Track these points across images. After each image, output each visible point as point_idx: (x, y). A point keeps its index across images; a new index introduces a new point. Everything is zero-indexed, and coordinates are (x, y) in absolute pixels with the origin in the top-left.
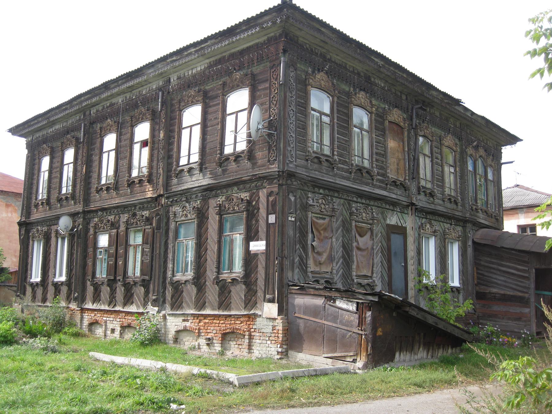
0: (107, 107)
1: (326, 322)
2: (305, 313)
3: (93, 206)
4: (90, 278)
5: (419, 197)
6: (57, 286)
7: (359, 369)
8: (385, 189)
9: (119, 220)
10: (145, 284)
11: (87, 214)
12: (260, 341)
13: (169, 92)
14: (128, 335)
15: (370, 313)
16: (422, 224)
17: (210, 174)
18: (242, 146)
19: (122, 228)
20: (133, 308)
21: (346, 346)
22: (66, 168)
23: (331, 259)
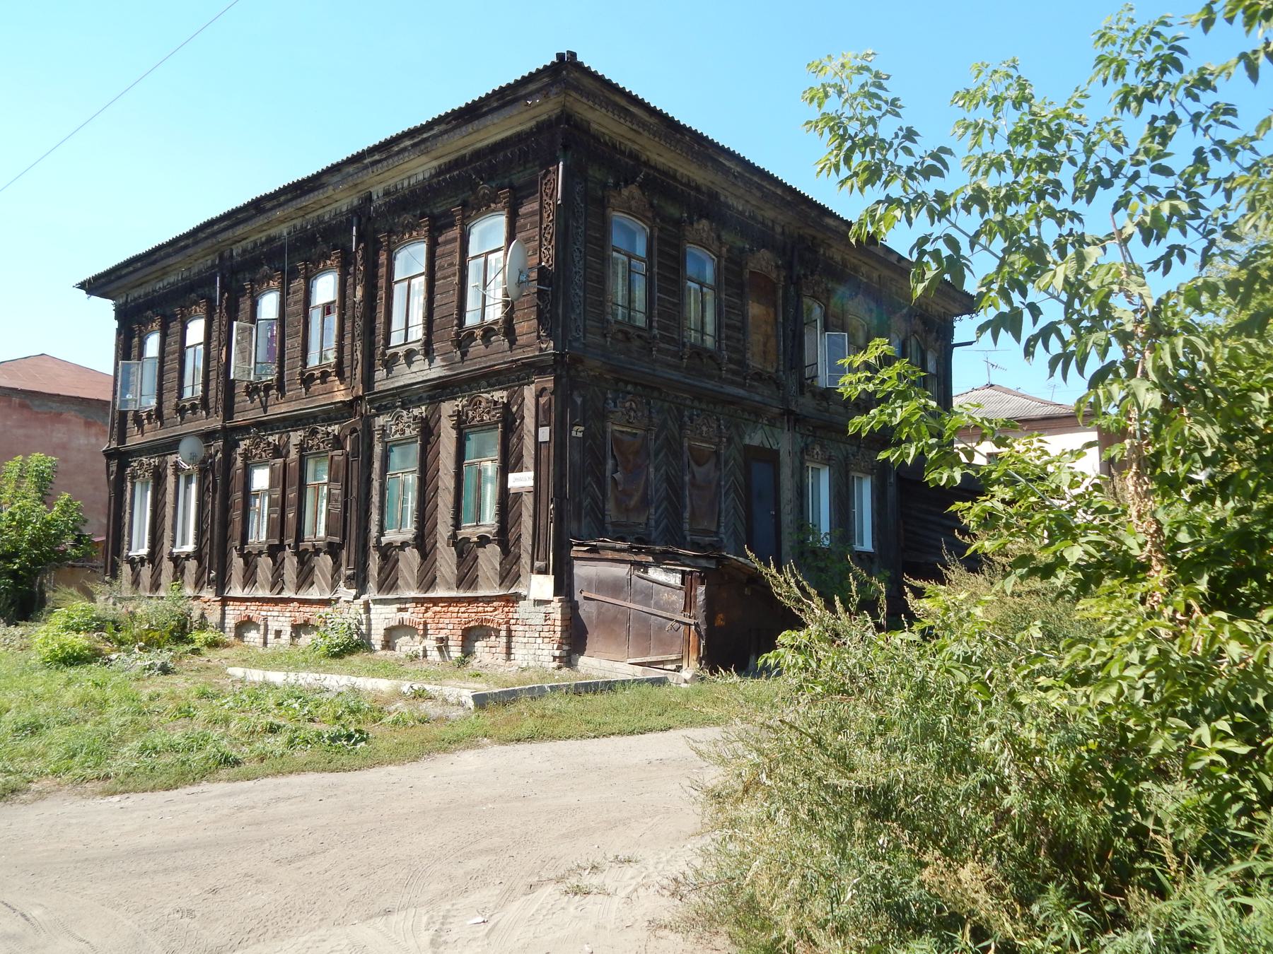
0: (263, 244)
1: (631, 605)
2: (598, 591)
3: (239, 419)
4: (237, 543)
5: (801, 400)
6: (177, 560)
7: (686, 681)
8: (742, 386)
9: (288, 442)
10: (333, 550)
11: (230, 435)
12: (525, 640)
13: (369, 219)
14: (305, 640)
15: (703, 588)
16: (807, 445)
17: (443, 360)
18: (495, 313)
19: (294, 454)
20: (313, 593)
21: (664, 645)
22: (190, 353)
23: (645, 502)
